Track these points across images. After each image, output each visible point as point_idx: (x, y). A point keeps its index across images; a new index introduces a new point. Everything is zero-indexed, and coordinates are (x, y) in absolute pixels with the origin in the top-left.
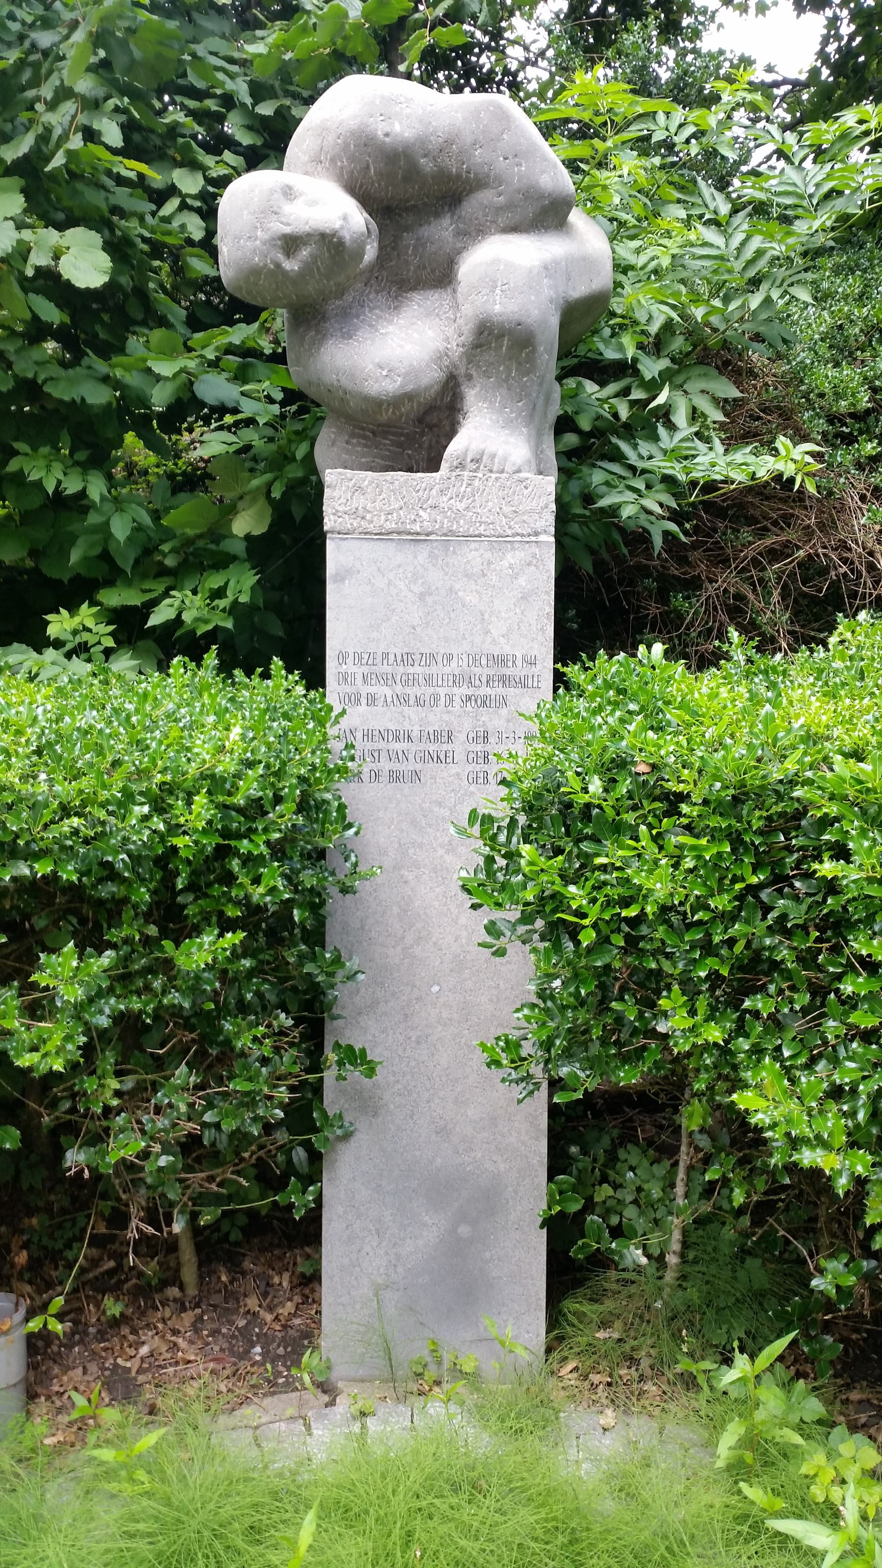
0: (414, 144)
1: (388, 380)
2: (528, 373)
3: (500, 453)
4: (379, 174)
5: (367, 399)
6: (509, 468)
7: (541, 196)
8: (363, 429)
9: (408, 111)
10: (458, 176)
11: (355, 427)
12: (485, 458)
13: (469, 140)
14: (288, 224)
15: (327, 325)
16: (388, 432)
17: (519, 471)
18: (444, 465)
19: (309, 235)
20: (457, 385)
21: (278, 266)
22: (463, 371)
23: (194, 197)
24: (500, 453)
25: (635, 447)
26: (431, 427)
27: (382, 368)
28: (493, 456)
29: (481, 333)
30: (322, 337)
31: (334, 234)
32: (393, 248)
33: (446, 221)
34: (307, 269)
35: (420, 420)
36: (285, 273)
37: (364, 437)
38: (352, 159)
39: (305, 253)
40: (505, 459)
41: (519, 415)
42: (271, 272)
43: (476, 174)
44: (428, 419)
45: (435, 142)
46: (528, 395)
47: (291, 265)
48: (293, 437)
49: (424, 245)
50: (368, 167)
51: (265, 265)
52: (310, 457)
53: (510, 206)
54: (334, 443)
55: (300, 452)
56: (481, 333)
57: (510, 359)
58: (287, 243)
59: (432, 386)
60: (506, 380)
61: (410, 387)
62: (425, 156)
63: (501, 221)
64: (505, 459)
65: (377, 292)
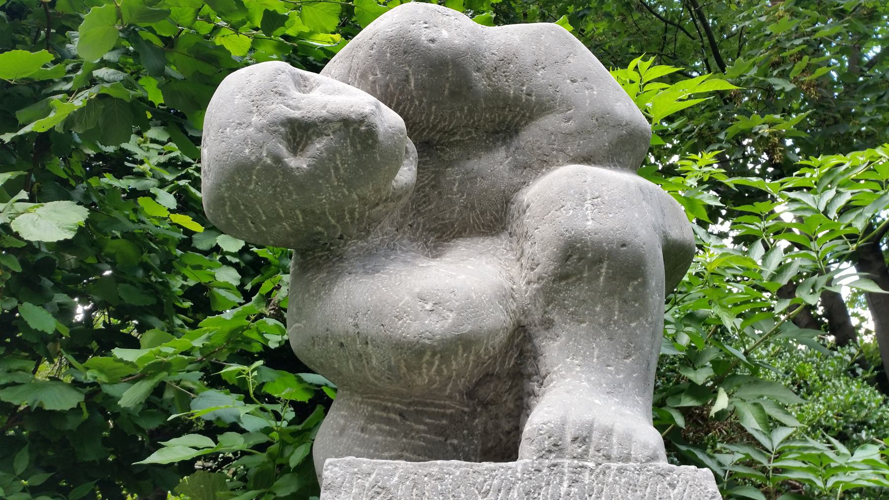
0: (465, 53)
1: (434, 317)
2: (637, 315)
4: (420, 86)
5: (400, 346)
7: (618, 125)
8: (385, 409)
10: (517, 98)
11: (375, 406)
12: (595, 435)
13: (530, 60)
14: (299, 108)
15: (346, 264)
16: (422, 413)
18: (526, 449)
19: (326, 121)
20: (528, 338)
21: (278, 159)
22: (537, 317)
23: (233, 255)
26: (485, 405)
27: (423, 299)
29: (568, 258)
30: (335, 275)
31: (362, 120)
32: (433, 187)
33: (500, 154)
34: (320, 170)
35: (471, 394)
36: (287, 171)
37: (389, 422)
38: (387, 70)
39: (318, 146)
42: (267, 169)
43: (538, 96)
44: (481, 392)
45: (489, 60)
47: (298, 163)
48: (289, 439)
50: (407, 80)
51: (259, 159)
52: (308, 460)
53: (581, 132)
54: (342, 431)
55: (295, 458)
56: (568, 258)
57: (611, 294)
58: (293, 133)
60: (605, 327)
61: (467, 328)
62: (478, 70)
65: (412, 241)
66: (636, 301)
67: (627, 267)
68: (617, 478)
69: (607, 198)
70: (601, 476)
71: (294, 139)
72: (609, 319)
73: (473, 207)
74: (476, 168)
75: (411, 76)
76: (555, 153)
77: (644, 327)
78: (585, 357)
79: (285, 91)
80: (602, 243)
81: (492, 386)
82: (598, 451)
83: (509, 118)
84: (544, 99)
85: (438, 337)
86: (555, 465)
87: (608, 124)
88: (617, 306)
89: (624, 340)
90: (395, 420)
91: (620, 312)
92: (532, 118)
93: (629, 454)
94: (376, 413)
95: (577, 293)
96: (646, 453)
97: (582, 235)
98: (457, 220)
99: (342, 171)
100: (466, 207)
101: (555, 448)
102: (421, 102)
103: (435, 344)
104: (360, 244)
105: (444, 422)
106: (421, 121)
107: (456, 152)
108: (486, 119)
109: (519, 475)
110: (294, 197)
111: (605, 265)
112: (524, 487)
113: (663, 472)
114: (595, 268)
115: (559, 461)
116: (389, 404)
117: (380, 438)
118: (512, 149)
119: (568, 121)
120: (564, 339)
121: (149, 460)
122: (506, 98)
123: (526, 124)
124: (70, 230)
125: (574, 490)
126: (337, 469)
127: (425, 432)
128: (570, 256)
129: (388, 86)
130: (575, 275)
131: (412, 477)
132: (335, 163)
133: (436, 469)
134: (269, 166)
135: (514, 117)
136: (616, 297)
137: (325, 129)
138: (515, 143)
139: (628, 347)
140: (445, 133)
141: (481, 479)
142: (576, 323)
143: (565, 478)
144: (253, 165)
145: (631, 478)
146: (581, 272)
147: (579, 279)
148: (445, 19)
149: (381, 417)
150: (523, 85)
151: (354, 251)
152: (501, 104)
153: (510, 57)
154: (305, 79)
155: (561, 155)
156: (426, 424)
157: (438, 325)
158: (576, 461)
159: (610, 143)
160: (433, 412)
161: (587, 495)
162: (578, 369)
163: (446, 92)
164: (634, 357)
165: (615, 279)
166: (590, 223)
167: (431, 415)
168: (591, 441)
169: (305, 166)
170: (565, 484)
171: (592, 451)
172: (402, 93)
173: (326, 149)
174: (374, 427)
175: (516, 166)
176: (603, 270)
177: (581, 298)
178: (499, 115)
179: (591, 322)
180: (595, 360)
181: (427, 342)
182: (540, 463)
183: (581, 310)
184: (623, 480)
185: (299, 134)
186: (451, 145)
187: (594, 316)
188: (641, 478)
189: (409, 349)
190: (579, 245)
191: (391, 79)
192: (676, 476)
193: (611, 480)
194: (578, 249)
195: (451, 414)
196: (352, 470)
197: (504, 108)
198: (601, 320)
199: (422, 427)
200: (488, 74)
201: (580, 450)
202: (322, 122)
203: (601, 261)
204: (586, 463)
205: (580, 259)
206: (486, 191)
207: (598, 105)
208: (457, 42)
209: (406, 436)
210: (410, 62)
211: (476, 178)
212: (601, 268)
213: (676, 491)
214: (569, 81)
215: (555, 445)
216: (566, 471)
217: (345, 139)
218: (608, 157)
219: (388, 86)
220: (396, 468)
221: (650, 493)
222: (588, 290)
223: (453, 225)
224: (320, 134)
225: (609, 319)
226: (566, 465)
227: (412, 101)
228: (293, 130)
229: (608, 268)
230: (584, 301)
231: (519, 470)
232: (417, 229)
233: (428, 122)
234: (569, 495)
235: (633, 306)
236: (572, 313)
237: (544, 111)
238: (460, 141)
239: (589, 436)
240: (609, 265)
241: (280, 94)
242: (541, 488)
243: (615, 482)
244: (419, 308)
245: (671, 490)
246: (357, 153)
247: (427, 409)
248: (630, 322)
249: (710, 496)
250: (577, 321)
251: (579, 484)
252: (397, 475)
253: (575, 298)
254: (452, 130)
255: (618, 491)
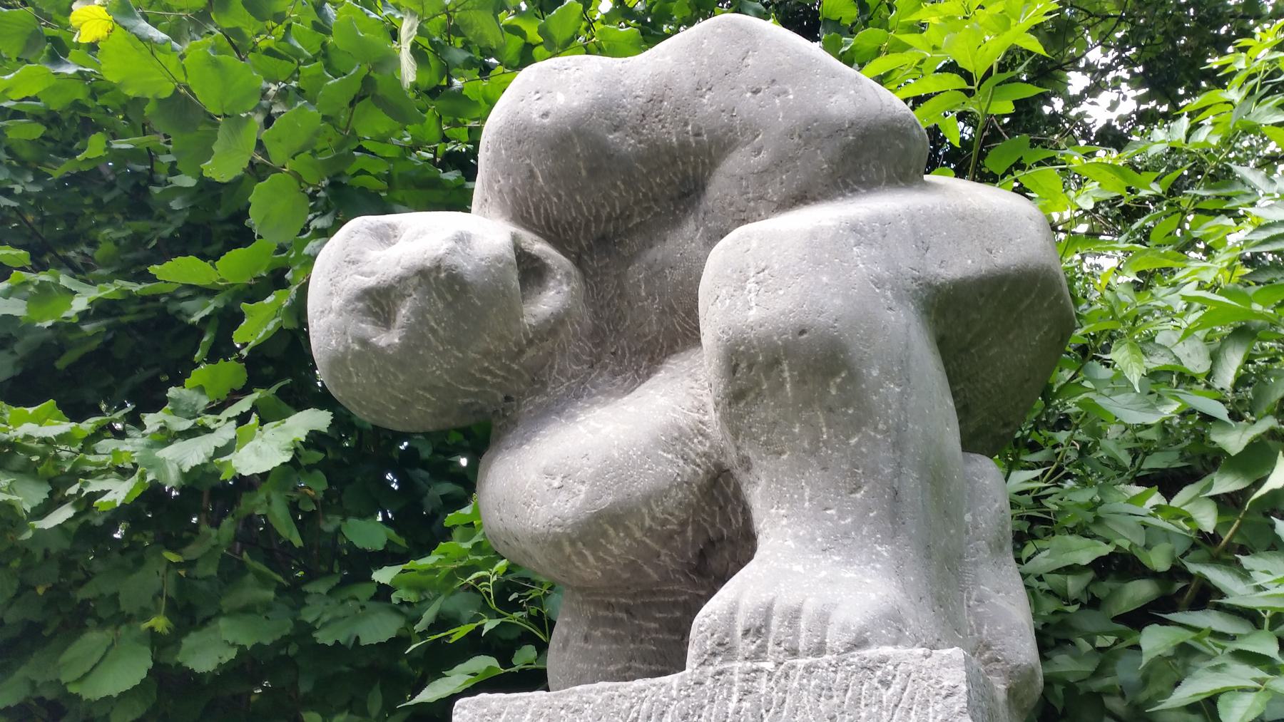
1: (563, 495)
2: (857, 424)
3: (811, 606)
4: (551, 177)
6: (834, 638)
7: (835, 130)
8: (609, 606)
9: (578, 74)
10: (684, 145)
11: (597, 604)
12: (775, 622)
14: (373, 273)
17: (860, 643)
19: (402, 279)
21: (364, 342)
24: (811, 606)
25: (1245, 575)
27: (550, 475)
28: (794, 616)
32: (621, 296)
34: (415, 338)
36: (379, 352)
37: (615, 623)
39: (404, 312)
40: (823, 619)
41: (862, 519)
42: (357, 355)
43: (710, 132)
46: (874, 472)
47: (388, 339)
49: (660, 274)
50: (532, 175)
51: (347, 348)
53: (781, 162)
56: (734, 369)
57: (808, 404)
58: (377, 304)
59: (664, 493)
60: (813, 452)
61: (607, 500)
62: (616, 129)
63: (774, 191)
64: (823, 619)
66: (847, 406)
67: (816, 360)
68: (805, 681)
69: (776, 267)
70: (783, 681)
71: (383, 309)
72: (816, 440)
73: (671, 307)
74: (659, 257)
75: (536, 169)
76: (752, 204)
77: (874, 439)
78: (792, 502)
79: (358, 257)
80: (770, 336)
81: (726, 555)
82: (779, 644)
83: (691, 172)
84: (719, 133)
85: (569, 522)
86: (720, 673)
87: (819, 136)
88: (822, 420)
89: (845, 467)
90: (622, 619)
91: (829, 426)
92: (713, 165)
93: (823, 643)
94: (600, 613)
95: (763, 415)
96: (846, 639)
97: (743, 332)
98: (659, 332)
99: (441, 332)
100: (663, 312)
101: (722, 649)
102: (559, 197)
103: (569, 531)
104: (538, 400)
105: (678, 614)
106: (575, 219)
107: (638, 239)
108: (659, 185)
109: (674, 693)
110: (402, 377)
111: (785, 366)
112: (680, 709)
113: (871, 665)
114: (774, 374)
115: (726, 666)
116: (613, 600)
117: (604, 647)
118: (701, 215)
119: (759, 153)
120: (763, 482)
121: (419, 699)
122: (669, 149)
123: (710, 174)
124: (288, 450)
125: (746, 705)
126: (466, 712)
127: (657, 631)
128: (737, 365)
129: (514, 190)
130: (751, 389)
131: (546, 711)
132: (428, 324)
133: (574, 698)
134: (359, 352)
135: (695, 168)
136: (816, 406)
137: (405, 289)
138: (703, 207)
139: (854, 474)
140: (617, 219)
141: (627, 704)
142: (774, 456)
143: (735, 689)
144: (344, 355)
145: (823, 679)
146: (758, 384)
147: (758, 395)
148: (562, 76)
149: (605, 618)
150: (686, 124)
151: (530, 412)
152: (667, 159)
153: (660, 93)
154: (393, 227)
155: (762, 204)
156: (656, 620)
157: (569, 505)
158: (748, 664)
159: (831, 162)
160: (663, 603)
161: (763, 711)
162: (785, 522)
163: (584, 173)
164: (865, 488)
165: (805, 382)
166: (752, 313)
167: (661, 607)
168: (768, 631)
169: (397, 340)
170: (735, 698)
171: (770, 645)
172: (532, 193)
173: (412, 313)
174: (598, 633)
175: (710, 239)
176: (786, 374)
177: (771, 420)
178: (675, 174)
179: (793, 450)
180: (807, 504)
181: (558, 530)
182: (701, 673)
183: (774, 437)
184: (813, 683)
185: (384, 302)
186: (630, 232)
187: (793, 441)
188: (840, 675)
189: (545, 541)
190: (742, 348)
191: (515, 180)
192: (891, 668)
193: (795, 684)
194: (743, 353)
195: (685, 602)
196: (480, 711)
197: (674, 162)
198: (806, 445)
199: (653, 625)
200: (634, 128)
201: (753, 647)
202: (399, 282)
203: (777, 362)
204: (762, 665)
205: (750, 367)
206: (682, 283)
207: (798, 114)
208: (575, 104)
209: (633, 641)
210: (527, 152)
211: (663, 270)
212: (782, 371)
213: (891, 691)
214: (749, 94)
215: (720, 644)
216: (736, 679)
217: (429, 293)
218: (835, 183)
219: (514, 190)
220: (528, 704)
221: (850, 699)
222: (775, 406)
223: (657, 340)
224: (403, 297)
225: (816, 440)
226: (736, 671)
227: (549, 199)
228: (373, 299)
229: (791, 370)
230: (775, 423)
231: (675, 686)
232: (624, 355)
233: (583, 215)
234: (738, 713)
235: (845, 414)
236: (766, 443)
237: (724, 149)
238: (641, 223)
239: (766, 624)
240: (790, 364)
241: (354, 263)
242: (702, 707)
243: (802, 687)
244: (546, 487)
245: (883, 691)
246: (449, 305)
247: (655, 599)
248: (848, 438)
249: (944, 693)
250: (775, 452)
251: (752, 696)
252: (530, 711)
253: (762, 422)
254: (622, 213)
255: (805, 700)
